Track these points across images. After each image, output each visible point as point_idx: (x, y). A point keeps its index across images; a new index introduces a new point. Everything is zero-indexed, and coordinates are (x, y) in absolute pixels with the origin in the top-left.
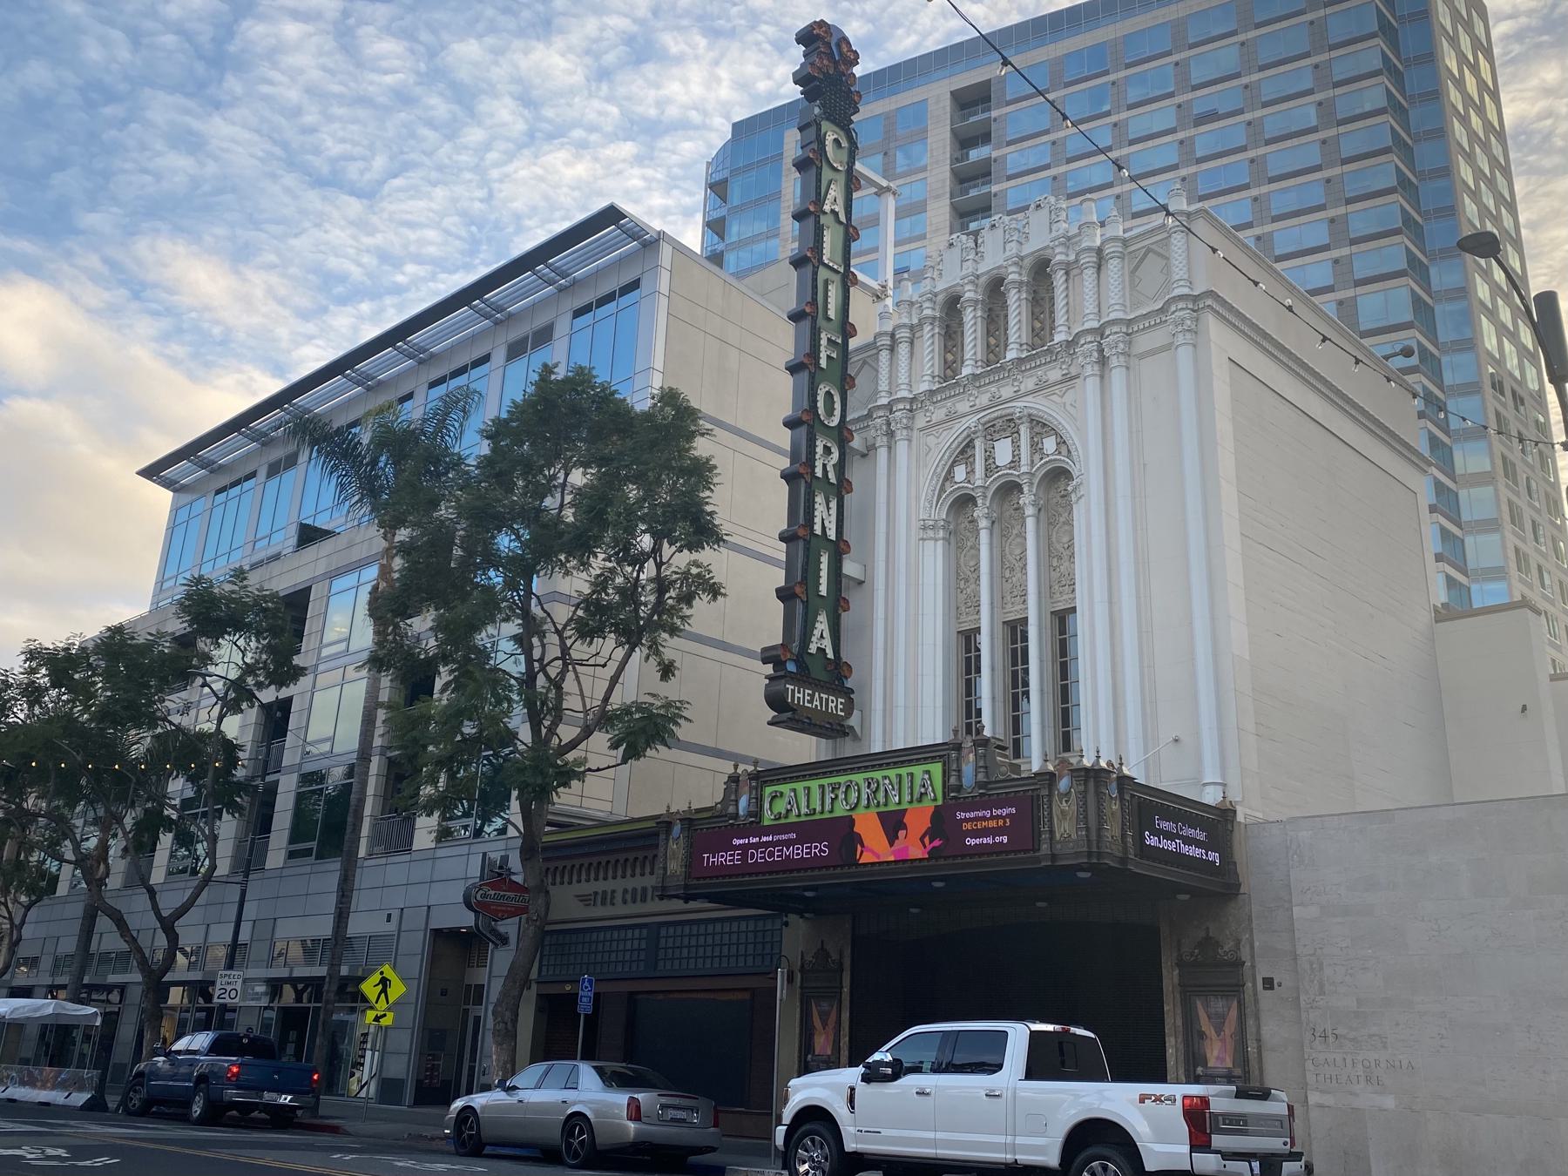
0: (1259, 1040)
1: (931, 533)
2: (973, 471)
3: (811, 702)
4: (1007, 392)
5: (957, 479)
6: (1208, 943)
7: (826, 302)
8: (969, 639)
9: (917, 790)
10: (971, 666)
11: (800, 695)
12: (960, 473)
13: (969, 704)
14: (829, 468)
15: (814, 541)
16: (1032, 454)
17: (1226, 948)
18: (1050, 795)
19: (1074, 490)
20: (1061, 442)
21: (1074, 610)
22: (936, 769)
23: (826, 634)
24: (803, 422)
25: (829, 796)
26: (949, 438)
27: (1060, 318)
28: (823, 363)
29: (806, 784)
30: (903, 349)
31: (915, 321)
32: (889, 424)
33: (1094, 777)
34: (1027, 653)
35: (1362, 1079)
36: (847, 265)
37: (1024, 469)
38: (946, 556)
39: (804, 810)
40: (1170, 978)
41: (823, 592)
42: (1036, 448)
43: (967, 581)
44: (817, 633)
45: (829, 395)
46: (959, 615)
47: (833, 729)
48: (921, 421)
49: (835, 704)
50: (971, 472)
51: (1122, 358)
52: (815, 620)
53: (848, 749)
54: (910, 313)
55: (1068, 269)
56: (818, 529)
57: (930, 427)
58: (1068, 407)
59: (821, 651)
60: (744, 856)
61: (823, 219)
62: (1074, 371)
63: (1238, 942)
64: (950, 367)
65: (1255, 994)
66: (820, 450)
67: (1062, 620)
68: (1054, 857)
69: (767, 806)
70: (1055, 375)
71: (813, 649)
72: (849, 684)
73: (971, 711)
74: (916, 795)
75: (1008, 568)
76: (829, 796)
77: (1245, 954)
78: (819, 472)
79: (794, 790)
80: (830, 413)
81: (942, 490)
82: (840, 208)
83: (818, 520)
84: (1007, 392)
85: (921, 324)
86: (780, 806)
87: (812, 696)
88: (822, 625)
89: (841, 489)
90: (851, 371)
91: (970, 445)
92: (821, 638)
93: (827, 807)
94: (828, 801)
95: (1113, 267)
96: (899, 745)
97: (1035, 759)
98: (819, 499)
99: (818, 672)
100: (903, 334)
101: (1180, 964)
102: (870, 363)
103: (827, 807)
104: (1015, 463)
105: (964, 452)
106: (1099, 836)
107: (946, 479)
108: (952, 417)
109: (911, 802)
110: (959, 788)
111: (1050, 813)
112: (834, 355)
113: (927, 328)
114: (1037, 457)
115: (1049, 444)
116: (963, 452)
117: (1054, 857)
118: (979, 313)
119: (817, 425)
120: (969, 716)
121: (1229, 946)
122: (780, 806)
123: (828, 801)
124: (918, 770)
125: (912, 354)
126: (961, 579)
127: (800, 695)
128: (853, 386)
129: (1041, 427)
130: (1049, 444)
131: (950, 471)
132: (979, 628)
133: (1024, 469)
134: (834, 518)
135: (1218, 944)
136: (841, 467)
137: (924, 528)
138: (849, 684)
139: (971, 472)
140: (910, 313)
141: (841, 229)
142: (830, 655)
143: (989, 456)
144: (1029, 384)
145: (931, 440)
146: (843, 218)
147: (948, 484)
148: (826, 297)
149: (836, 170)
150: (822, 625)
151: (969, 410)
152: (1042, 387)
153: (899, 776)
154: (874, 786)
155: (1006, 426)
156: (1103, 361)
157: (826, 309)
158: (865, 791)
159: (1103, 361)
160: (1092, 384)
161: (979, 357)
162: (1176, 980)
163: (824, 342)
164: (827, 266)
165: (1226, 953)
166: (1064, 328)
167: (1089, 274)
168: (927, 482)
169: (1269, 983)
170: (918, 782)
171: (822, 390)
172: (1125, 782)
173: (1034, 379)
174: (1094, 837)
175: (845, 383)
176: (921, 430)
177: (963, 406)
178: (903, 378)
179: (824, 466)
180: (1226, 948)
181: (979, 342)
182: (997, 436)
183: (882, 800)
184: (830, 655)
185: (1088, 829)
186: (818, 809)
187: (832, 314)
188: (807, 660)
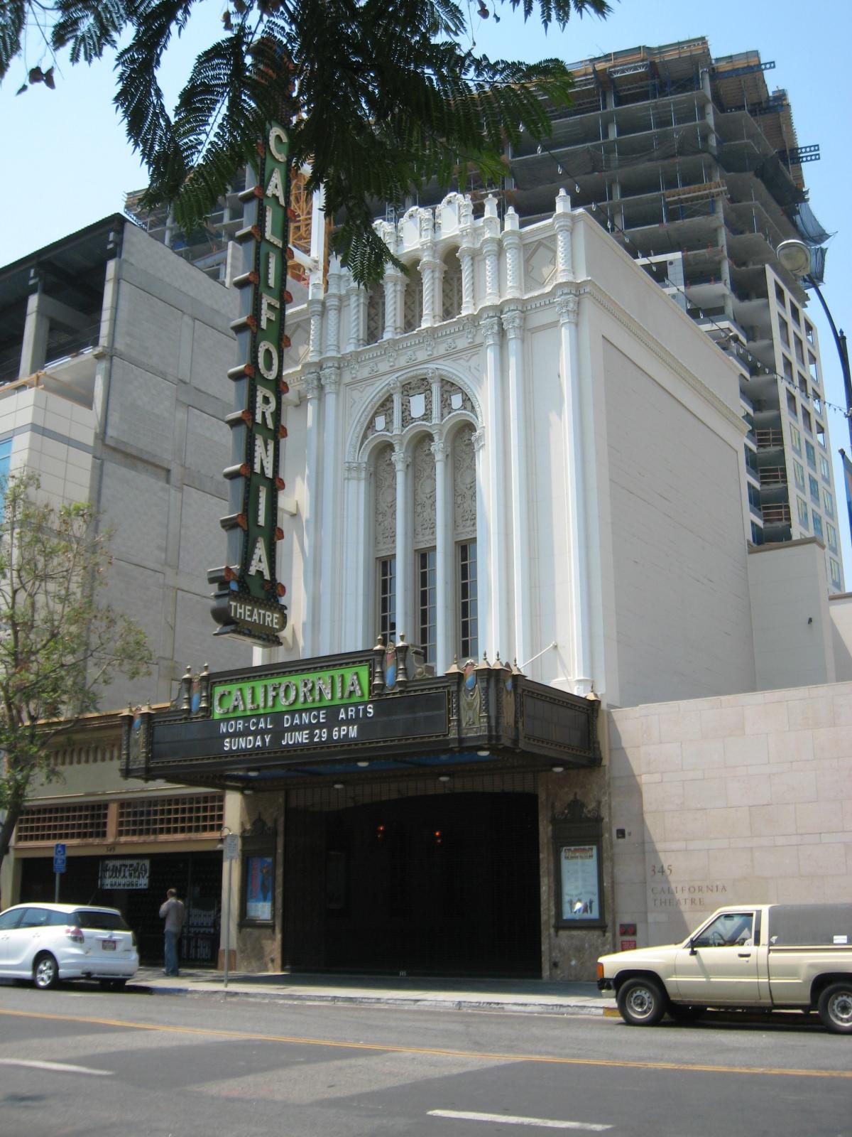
0: (612, 878)
1: (354, 474)
2: (391, 421)
3: (251, 616)
4: (422, 355)
5: (454, 406)
6: (576, 805)
7: (267, 273)
8: (385, 565)
9: (348, 688)
10: (386, 586)
11: (242, 611)
12: (380, 422)
13: (384, 619)
14: (268, 416)
15: (254, 479)
16: (442, 408)
17: (590, 807)
18: (459, 691)
19: (477, 440)
20: (467, 399)
21: (474, 540)
22: (364, 672)
23: (264, 558)
24: (250, 377)
25: (271, 693)
26: (369, 396)
27: (466, 298)
28: (264, 324)
29: (252, 684)
30: (332, 315)
31: (343, 292)
32: (319, 379)
33: (493, 677)
34: (430, 573)
35: (688, 902)
36: (286, 242)
37: (435, 421)
38: (367, 494)
39: (249, 706)
40: (545, 831)
41: (262, 520)
42: (446, 404)
43: (384, 515)
44: (256, 557)
45: (268, 352)
46: (376, 542)
47: (270, 638)
48: (347, 378)
49: (272, 619)
50: (389, 423)
51: (333, 387)
52: (254, 547)
53: (281, 655)
54: (339, 286)
55: (475, 255)
56: (257, 469)
57: (355, 382)
58: (473, 370)
59: (260, 573)
60: (311, 736)
61: (265, 202)
62: (478, 340)
63: (599, 803)
64: (373, 332)
65: (611, 843)
66: (259, 399)
67: (465, 551)
68: (461, 740)
69: (216, 703)
70: (462, 343)
71: (252, 571)
72: (283, 601)
73: (387, 626)
74: (347, 694)
75: (420, 505)
76: (271, 693)
77: (604, 813)
78: (259, 419)
79: (241, 690)
80: (269, 367)
81: (365, 437)
82: (280, 193)
83: (257, 460)
84: (422, 355)
85: (348, 295)
86: (229, 703)
87: (252, 612)
88: (260, 550)
89: (278, 433)
90: (287, 332)
91: (389, 399)
92: (259, 563)
93: (270, 703)
94: (270, 699)
95: (510, 258)
96: (325, 651)
97: (443, 665)
98: (259, 442)
99: (256, 591)
100: (333, 302)
101: (554, 821)
102: (303, 325)
103: (270, 703)
104: (427, 416)
105: (385, 406)
106: (498, 723)
107: (368, 428)
108: (376, 376)
109: (342, 697)
110: (383, 686)
111: (458, 706)
112: (273, 318)
113: (353, 299)
114: (446, 411)
115: (456, 401)
116: (383, 405)
117: (461, 740)
118: (399, 288)
119: (258, 379)
120: (384, 628)
121: (592, 805)
122: (229, 703)
123: (270, 699)
124: (349, 673)
125: (339, 317)
126: (379, 515)
127: (242, 611)
128: (289, 345)
129: (449, 386)
130: (456, 401)
131: (371, 425)
132: (435, 547)
133: (396, 432)
134: (271, 459)
135: (583, 805)
136: (277, 415)
137: (349, 469)
138: (283, 601)
139: (389, 423)
140: (339, 286)
141: (281, 211)
142: (267, 577)
143: (406, 409)
144: (442, 350)
145: (356, 394)
146: (282, 201)
147: (369, 432)
148: (267, 268)
149: (277, 161)
150: (260, 550)
151: (385, 372)
152: (452, 354)
153: (332, 678)
154: (310, 686)
155: (422, 385)
156: (502, 333)
157: (267, 278)
158: (302, 690)
159: (502, 333)
160: (491, 355)
161: (361, 337)
162: (550, 834)
163: (264, 306)
164: (268, 241)
165: (589, 812)
166: (471, 305)
167: (489, 265)
168: (353, 431)
169: (621, 833)
170: (348, 682)
171: (263, 346)
172: (518, 679)
173: (445, 346)
174: (493, 723)
175: (282, 342)
176: (347, 385)
177: (383, 367)
178: (332, 340)
179: (264, 413)
180: (590, 807)
181: (362, 323)
182: (411, 392)
183: (317, 698)
184: (267, 577)
185: (489, 717)
186: (262, 705)
187: (272, 282)
188: (248, 580)
